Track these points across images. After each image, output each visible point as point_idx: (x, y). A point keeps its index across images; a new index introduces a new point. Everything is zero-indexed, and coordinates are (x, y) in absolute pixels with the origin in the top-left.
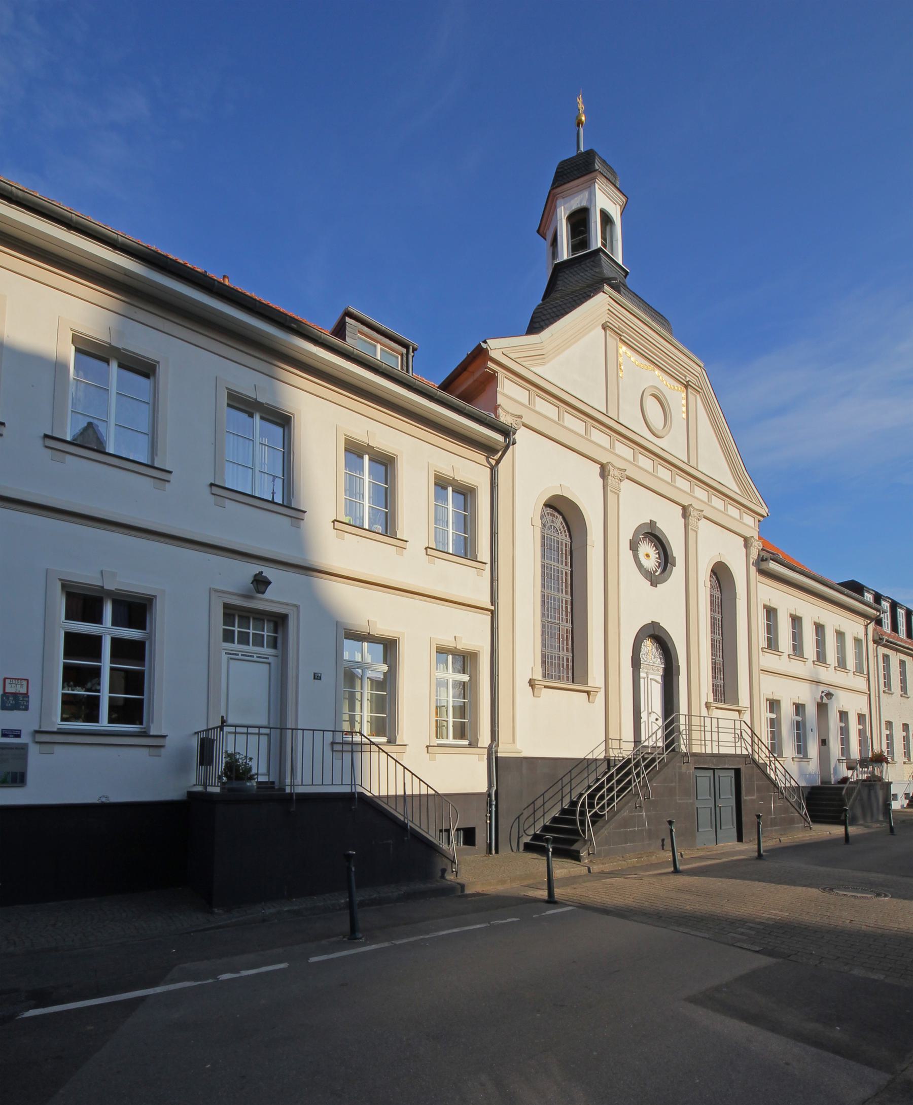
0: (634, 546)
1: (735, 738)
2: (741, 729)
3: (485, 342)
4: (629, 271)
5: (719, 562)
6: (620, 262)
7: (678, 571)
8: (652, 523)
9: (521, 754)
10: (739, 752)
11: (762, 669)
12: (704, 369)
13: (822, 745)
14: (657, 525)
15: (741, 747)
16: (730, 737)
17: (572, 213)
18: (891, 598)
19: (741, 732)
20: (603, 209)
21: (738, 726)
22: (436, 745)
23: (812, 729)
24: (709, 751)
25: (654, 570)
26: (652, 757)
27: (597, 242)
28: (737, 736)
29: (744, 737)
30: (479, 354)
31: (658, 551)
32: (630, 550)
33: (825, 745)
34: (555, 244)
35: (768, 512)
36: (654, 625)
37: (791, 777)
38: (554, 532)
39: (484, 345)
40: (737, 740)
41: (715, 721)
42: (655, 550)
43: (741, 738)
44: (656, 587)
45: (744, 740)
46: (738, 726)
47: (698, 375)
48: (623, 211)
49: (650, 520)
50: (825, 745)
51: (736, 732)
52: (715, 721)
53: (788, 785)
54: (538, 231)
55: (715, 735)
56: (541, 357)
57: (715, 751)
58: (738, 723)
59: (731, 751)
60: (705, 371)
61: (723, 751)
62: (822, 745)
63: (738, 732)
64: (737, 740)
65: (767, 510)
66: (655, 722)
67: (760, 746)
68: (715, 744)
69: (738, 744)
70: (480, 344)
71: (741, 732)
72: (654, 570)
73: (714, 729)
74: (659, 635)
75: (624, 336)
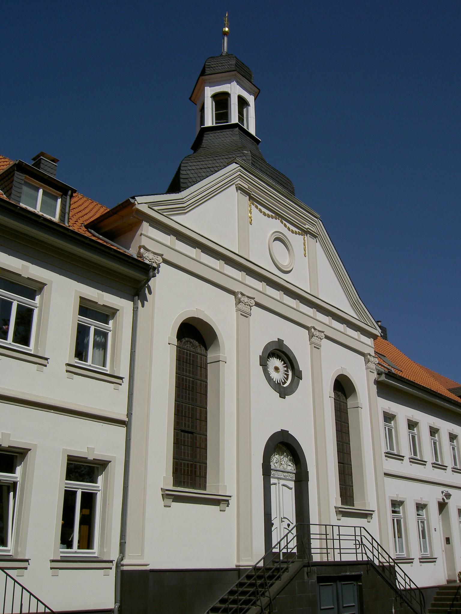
0: (263, 363)
1: (356, 544)
2: (361, 536)
3: (133, 198)
4: (260, 140)
5: (342, 374)
6: (252, 130)
7: (305, 384)
8: (280, 342)
9: (148, 567)
10: (360, 559)
11: (387, 472)
12: (320, 220)
13: (447, 544)
14: (284, 343)
15: (362, 553)
16: (351, 544)
17: (216, 94)
18: (290, 543)
19: (361, 538)
20: (240, 95)
21: (358, 533)
22: (59, 558)
23: (435, 529)
24: (331, 559)
25: (283, 381)
26: (269, 573)
27: (234, 119)
28: (357, 543)
29: (364, 543)
30: (128, 205)
31: (286, 365)
32: (260, 365)
33: (449, 543)
34: (203, 111)
35: (381, 332)
36: (284, 433)
37: (410, 580)
38: (190, 347)
39: (132, 201)
40: (358, 546)
41: (336, 529)
42: (283, 364)
43: (361, 545)
44: (284, 398)
45: (364, 545)
46: (358, 533)
47: (316, 224)
48: (257, 97)
49: (278, 339)
50: (449, 543)
51: (356, 539)
52: (336, 529)
53: (408, 587)
54: (190, 99)
55: (337, 543)
56: (183, 210)
57: (337, 559)
58: (358, 530)
59: (352, 558)
60: (321, 221)
61: (346, 558)
62: (447, 544)
63: (358, 538)
64: (358, 546)
65: (380, 331)
66: (290, 524)
67: (380, 551)
68: (337, 551)
69: (359, 551)
70: (129, 199)
71: (361, 538)
72: (283, 381)
73: (336, 537)
74: (288, 442)
75: (253, 194)
